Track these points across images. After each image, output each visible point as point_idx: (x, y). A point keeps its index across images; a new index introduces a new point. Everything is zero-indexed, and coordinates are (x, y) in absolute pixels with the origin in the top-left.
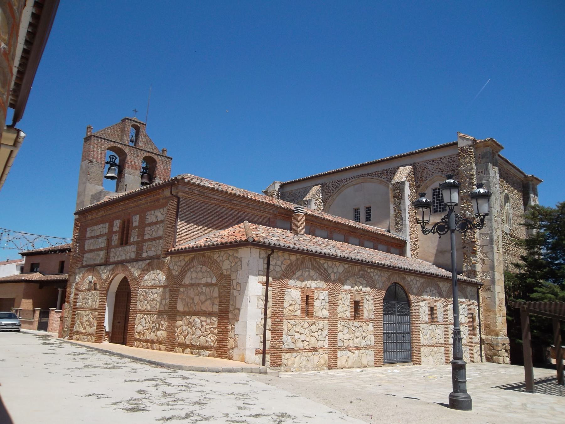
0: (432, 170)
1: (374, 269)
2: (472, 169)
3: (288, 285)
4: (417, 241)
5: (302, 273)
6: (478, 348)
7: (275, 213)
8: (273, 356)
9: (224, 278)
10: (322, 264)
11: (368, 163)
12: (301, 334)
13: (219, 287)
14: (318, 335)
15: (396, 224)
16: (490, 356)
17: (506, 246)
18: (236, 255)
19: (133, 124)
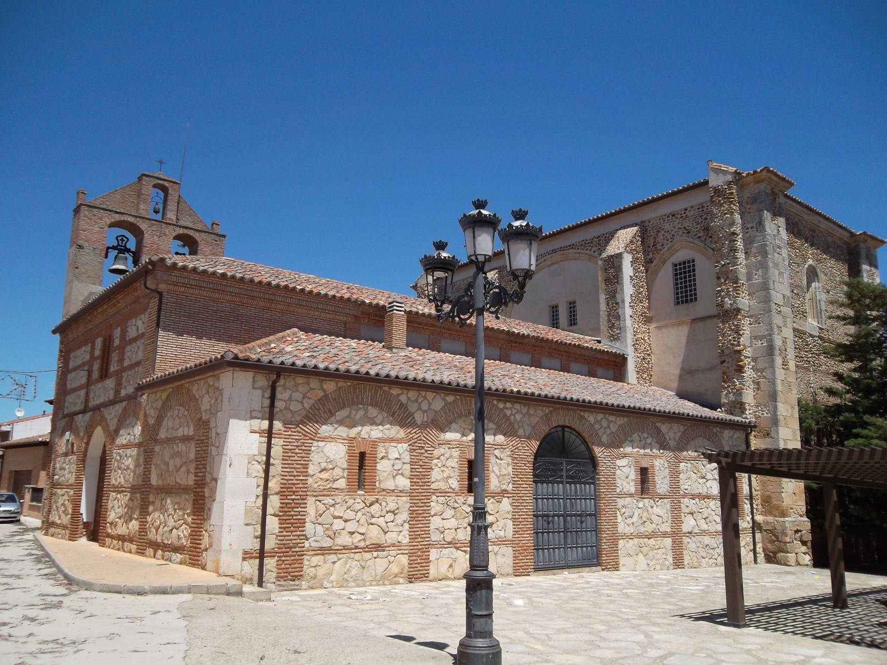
0: (672, 230)
1: (513, 403)
2: (733, 224)
3: (318, 435)
4: (649, 355)
5: (350, 412)
6: (748, 539)
7: (356, 313)
8: (283, 561)
9: (202, 427)
10: (395, 396)
11: (569, 227)
12: (346, 521)
13: (197, 442)
14: (387, 523)
15: (609, 327)
16: (772, 552)
17: (811, 357)
18: (216, 385)
19: (155, 182)
